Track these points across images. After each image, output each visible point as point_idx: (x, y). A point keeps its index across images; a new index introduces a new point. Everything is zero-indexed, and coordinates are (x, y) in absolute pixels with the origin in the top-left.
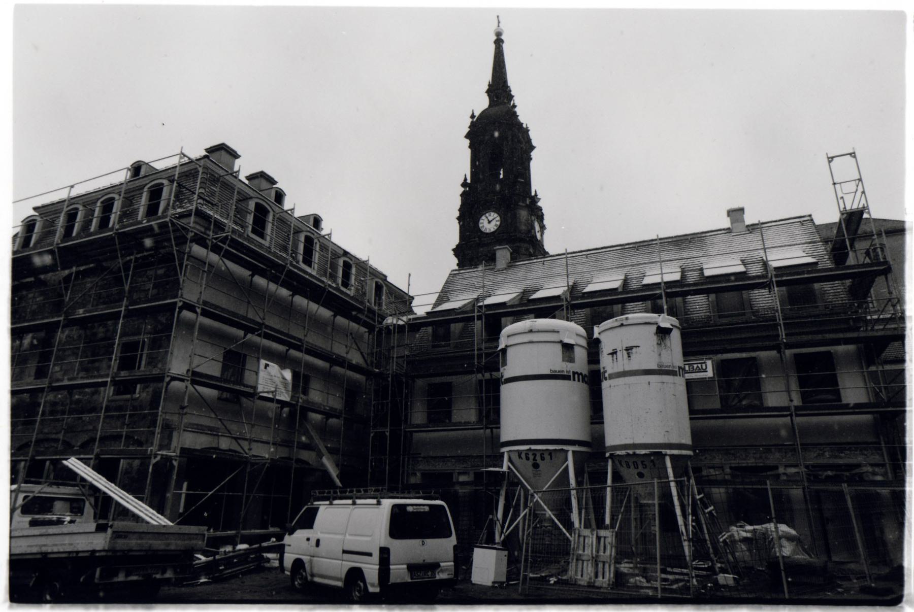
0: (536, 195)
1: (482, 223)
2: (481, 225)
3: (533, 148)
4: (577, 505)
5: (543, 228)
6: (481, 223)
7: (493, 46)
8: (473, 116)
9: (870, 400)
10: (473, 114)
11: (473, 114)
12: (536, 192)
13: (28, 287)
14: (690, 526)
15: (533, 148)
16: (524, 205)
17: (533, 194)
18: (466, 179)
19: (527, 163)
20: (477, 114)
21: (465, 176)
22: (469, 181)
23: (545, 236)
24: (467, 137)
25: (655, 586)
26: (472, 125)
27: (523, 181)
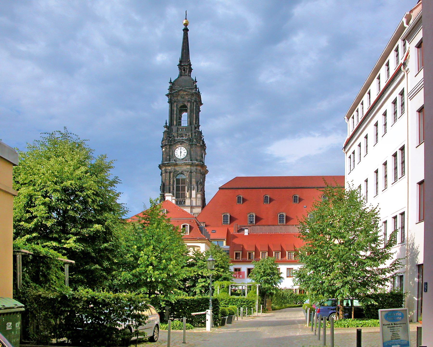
8: (171, 82)
10: (171, 80)
16: (200, 145)
18: (166, 123)
21: (166, 121)
26: (171, 89)
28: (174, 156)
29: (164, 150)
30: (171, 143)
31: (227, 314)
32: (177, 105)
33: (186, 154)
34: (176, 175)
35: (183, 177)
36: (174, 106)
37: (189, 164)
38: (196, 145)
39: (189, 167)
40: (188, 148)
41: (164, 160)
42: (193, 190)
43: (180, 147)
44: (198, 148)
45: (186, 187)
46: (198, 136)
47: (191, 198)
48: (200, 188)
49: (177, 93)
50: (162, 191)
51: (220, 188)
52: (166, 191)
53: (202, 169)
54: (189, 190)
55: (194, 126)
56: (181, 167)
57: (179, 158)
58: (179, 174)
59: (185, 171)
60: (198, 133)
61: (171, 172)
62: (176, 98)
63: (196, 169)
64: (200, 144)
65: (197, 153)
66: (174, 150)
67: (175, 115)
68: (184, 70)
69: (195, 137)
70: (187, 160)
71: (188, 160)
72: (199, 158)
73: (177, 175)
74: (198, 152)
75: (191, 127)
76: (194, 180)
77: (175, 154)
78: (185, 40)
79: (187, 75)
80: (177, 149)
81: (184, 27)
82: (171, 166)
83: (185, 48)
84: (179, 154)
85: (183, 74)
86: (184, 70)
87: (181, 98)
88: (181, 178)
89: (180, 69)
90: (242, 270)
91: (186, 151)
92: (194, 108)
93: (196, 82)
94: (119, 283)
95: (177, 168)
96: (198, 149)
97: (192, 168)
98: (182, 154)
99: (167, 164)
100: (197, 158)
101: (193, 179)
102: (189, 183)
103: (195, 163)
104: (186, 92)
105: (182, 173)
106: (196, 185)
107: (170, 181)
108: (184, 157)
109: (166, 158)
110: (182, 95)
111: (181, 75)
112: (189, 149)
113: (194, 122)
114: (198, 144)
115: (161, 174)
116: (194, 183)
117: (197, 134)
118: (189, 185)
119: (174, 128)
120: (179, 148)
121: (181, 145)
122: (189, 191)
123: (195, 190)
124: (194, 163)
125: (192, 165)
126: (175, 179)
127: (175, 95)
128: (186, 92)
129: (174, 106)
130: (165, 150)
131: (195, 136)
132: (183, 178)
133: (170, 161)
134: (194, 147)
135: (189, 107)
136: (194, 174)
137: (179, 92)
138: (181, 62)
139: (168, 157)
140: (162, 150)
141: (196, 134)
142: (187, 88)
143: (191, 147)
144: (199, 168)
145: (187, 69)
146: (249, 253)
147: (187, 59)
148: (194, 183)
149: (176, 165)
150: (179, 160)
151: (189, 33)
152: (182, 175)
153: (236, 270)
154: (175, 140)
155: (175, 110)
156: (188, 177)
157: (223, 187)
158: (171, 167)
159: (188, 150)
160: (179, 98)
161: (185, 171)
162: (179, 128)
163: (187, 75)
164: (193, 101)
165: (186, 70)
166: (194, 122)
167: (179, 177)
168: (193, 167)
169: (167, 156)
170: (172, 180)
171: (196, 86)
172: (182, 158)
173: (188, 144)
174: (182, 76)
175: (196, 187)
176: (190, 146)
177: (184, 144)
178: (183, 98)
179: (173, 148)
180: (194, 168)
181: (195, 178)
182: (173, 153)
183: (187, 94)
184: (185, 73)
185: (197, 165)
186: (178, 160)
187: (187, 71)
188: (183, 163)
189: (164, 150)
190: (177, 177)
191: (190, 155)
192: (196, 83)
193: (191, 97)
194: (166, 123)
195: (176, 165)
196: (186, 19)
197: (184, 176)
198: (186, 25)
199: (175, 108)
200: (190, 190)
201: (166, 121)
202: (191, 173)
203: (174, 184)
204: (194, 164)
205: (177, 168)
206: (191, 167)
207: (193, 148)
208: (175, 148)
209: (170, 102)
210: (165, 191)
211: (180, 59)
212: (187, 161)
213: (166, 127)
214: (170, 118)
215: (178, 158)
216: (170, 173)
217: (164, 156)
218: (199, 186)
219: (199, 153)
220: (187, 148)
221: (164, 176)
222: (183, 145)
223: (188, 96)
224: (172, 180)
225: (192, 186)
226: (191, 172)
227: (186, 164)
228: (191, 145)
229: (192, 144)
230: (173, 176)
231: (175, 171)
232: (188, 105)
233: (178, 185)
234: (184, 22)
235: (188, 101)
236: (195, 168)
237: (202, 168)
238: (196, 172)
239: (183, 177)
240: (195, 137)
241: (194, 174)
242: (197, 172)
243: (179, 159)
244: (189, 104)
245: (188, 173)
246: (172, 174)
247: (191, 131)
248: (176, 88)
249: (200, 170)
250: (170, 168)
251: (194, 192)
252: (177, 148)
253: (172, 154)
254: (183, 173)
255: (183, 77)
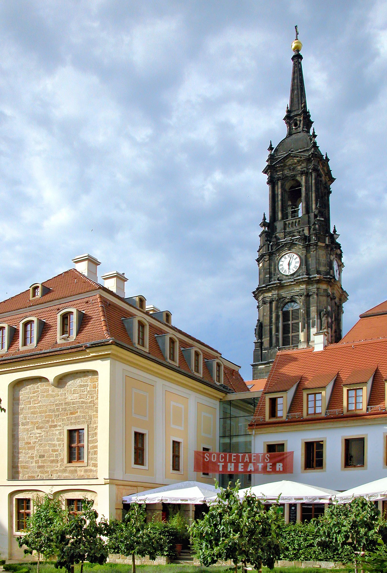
0: (335, 231)
1: (282, 265)
2: (281, 263)
3: (332, 180)
4: (153, 376)
5: (341, 265)
6: (282, 265)
7: (291, 63)
8: (271, 148)
9: (254, 475)
10: (271, 145)
11: (271, 145)
12: (335, 227)
13: (71, 501)
14: (72, 416)
15: (332, 180)
16: (324, 245)
17: (332, 231)
18: (265, 219)
19: (326, 198)
20: (275, 146)
22: (268, 221)
23: (343, 274)
24: (265, 172)
25: (36, 295)
26: (271, 158)
27: (323, 219)
28: (278, 273)
29: (261, 265)
30: (272, 250)
31: (6, 535)
32: (282, 185)
33: (298, 265)
34: (282, 305)
35: (296, 306)
36: (278, 187)
37: (303, 281)
38: (316, 245)
39: (303, 287)
40: (302, 254)
41: (262, 282)
42: (313, 327)
43: (287, 254)
44: (320, 251)
45: (300, 323)
46: (319, 230)
47: (308, 343)
48: (326, 321)
49: (282, 163)
50: (257, 336)
51: (362, 317)
52: (265, 335)
53: (329, 287)
54: (304, 328)
55: (313, 214)
56: (290, 289)
57: (287, 274)
58: (288, 302)
59: (297, 295)
60: (320, 223)
61: (273, 301)
62: (281, 173)
63: (318, 289)
64: (324, 242)
65: (319, 260)
66: (277, 262)
67: (280, 203)
68: (296, 125)
69: (314, 232)
70: (301, 274)
71: (303, 275)
72: (323, 269)
73: (285, 305)
74: (321, 259)
75: (309, 217)
76: (313, 309)
77: (280, 267)
78: (296, 75)
79: (300, 132)
80: (283, 259)
81: (293, 54)
82: (273, 289)
83: (296, 87)
84: (286, 267)
85: (294, 131)
86: (296, 125)
87: (290, 170)
88: (290, 309)
89: (287, 123)
90: (288, 449)
91: (298, 260)
92: (313, 181)
93: (315, 136)
94: (265, 517)
95: (284, 293)
96: (322, 253)
97: (310, 287)
98: (291, 267)
99: (265, 288)
100: (320, 269)
101: (313, 306)
102: (306, 316)
103: (315, 277)
104: (298, 157)
105: (292, 300)
106: (319, 317)
107: (271, 318)
108: (295, 270)
109: (265, 277)
110: (292, 165)
111: (290, 134)
112: (304, 256)
113: (314, 206)
114: (320, 244)
115: (258, 307)
116: (314, 314)
117: (319, 226)
118: (304, 319)
119: (279, 225)
120: (286, 256)
121: (289, 250)
122: (305, 330)
123: (315, 326)
124: (313, 278)
125: (309, 282)
126: (280, 313)
127: (279, 167)
128: (297, 158)
129: (278, 187)
130: (263, 265)
131: (314, 229)
132: (294, 309)
133: (270, 282)
134: (313, 250)
135: (303, 183)
136: (313, 298)
137: (284, 161)
138: (289, 112)
139: (268, 276)
140: (259, 266)
141: (317, 226)
142: (299, 151)
143: (308, 251)
144: (324, 286)
145: (300, 121)
146: (270, 399)
147: (300, 105)
148: (314, 314)
149: (281, 286)
150: (287, 277)
151: (303, 62)
152: (292, 304)
153: (271, 448)
154: (277, 244)
155: (280, 193)
156: (303, 305)
157: (370, 312)
158: (273, 291)
159: (302, 257)
160: (286, 172)
161: (297, 295)
162: (287, 222)
163: (300, 132)
164: (310, 171)
165: (298, 123)
166: (314, 206)
167: (290, 308)
168: (312, 286)
169: (266, 274)
170: (274, 315)
171: (315, 143)
172: (292, 272)
173: (301, 247)
174: (292, 135)
175: (319, 320)
176: (305, 249)
177: (295, 247)
178: (294, 169)
179: (276, 259)
180: (313, 288)
181: (316, 305)
182: (277, 267)
183: (299, 161)
184: (297, 128)
185: (318, 282)
186: (284, 277)
187: (300, 124)
188: (292, 282)
189: (261, 265)
190: (284, 309)
191: (307, 264)
192: (316, 139)
193: (307, 165)
194: (265, 219)
195: (281, 286)
196: (297, 39)
197: (296, 304)
198: (297, 49)
199: (280, 190)
200: (308, 326)
201: (264, 215)
202: (308, 298)
203: (279, 322)
204: (312, 279)
205: (284, 293)
206: (308, 287)
207: (312, 252)
208: (279, 258)
209: (272, 182)
210: (263, 337)
211: (288, 108)
212: (300, 276)
213: (264, 224)
214: (271, 210)
215: (285, 274)
216: (271, 303)
217: (262, 276)
218: (323, 319)
219: (323, 260)
220: (299, 254)
221: (262, 310)
222: (293, 250)
223: (301, 165)
224: (274, 315)
225: (310, 320)
226: (308, 296)
227: (299, 283)
228: (307, 248)
229: (309, 245)
230: (277, 308)
231: (280, 299)
232: (302, 179)
233: (286, 323)
234: (294, 45)
235: (302, 173)
236: (315, 286)
237: (331, 286)
238: (317, 295)
239: (294, 306)
240: (314, 232)
241: (314, 299)
242: (319, 294)
243: (287, 276)
244: (304, 178)
245: (303, 298)
246: (274, 304)
247: (309, 222)
248: (280, 155)
249: (326, 290)
250: (270, 294)
251: (313, 331)
252: (282, 256)
253: (275, 270)
254: (294, 300)
255: (293, 136)
